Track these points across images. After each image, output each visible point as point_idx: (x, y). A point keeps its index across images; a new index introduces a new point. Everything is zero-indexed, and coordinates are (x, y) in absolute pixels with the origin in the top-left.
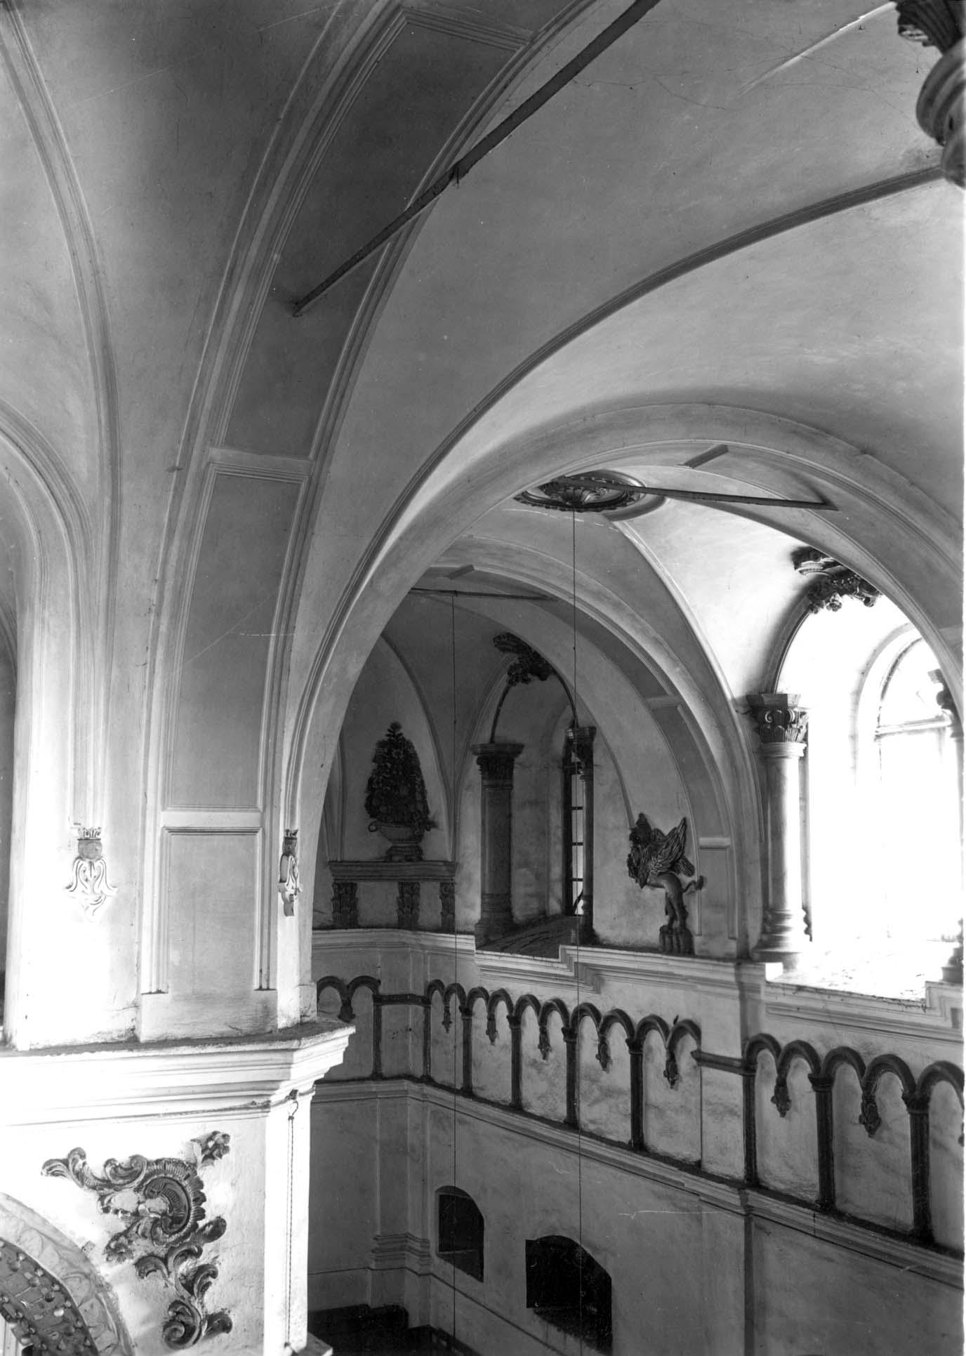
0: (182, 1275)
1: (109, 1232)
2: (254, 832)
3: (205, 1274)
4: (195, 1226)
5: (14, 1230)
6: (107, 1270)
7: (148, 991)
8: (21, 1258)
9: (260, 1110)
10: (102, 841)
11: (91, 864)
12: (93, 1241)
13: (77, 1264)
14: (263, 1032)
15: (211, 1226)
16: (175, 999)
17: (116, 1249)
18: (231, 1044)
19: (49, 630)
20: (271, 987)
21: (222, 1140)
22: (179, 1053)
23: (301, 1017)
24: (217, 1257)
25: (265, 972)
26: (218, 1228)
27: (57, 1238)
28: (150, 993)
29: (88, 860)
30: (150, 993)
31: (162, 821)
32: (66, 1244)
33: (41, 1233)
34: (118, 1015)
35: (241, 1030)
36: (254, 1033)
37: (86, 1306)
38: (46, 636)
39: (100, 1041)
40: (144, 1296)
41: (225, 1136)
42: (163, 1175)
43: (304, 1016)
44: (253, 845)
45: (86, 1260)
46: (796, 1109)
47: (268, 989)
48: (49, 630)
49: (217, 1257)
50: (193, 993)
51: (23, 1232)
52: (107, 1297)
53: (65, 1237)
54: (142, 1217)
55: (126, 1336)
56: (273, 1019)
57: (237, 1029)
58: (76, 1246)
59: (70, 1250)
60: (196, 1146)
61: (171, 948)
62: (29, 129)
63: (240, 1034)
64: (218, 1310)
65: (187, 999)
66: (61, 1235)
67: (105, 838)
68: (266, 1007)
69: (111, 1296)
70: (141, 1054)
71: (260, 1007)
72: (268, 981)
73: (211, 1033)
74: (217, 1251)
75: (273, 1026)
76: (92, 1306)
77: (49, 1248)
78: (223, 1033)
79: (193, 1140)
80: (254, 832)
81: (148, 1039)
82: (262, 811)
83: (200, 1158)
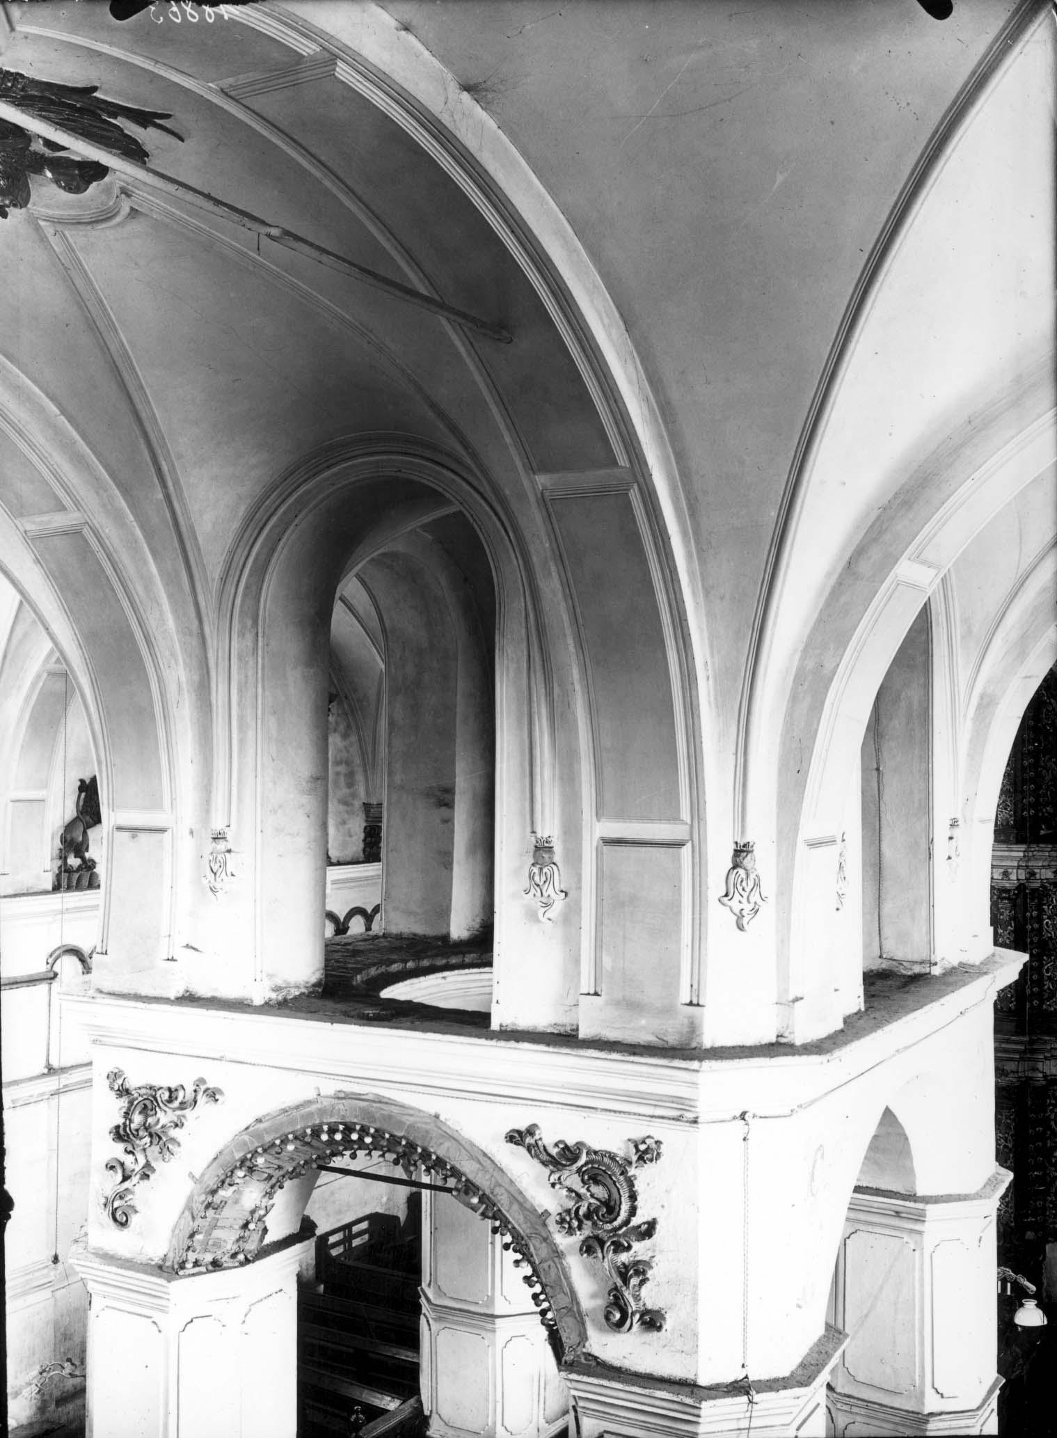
0: (623, 1264)
1: (562, 1206)
2: (680, 844)
3: (639, 1270)
4: (627, 1222)
5: (488, 1183)
6: (563, 1241)
7: (587, 992)
8: (495, 1209)
9: (688, 1124)
10: (555, 849)
11: (541, 869)
12: (550, 1211)
13: (537, 1227)
14: (688, 1047)
15: (646, 1226)
16: (607, 1004)
17: (568, 1221)
18: (634, 1054)
19: (507, 656)
20: (701, 1003)
21: (654, 1146)
22: (587, 1054)
23: (778, 1036)
24: (653, 1257)
25: (695, 986)
26: (648, 1230)
27: (521, 1200)
28: (589, 994)
29: (538, 866)
30: (589, 994)
31: (598, 831)
32: (528, 1206)
33: (508, 1192)
34: (570, 1010)
35: (667, 1042)
36: (679, 1047)
37: (545, 1265)
38: (505, 662)
39: (556, 1032)
40: (593, 1273)
41: (658, 1143)
42: (597, 1166)
43: (782, 1036)
44: (678, 859)
45: (545, 1225)
46: (420, 6)
47: (698, 1005)
48: (507, 656)
49: (653, 1257)
50: (624, 999)
51: (495, 1186)
52: (561, 1264)
53: (527, 1200)
54: (583, 1200)
55: (578, 1304)
56: (699, 1035)
57: (664, 1040)
58: (536, 1210)
59: (531, 1212)
60: (631, 1146)
61: (604, 953)
62: (646, 382)
63: (666, 1046)
64: (656, 1308)
65: (617, 1003)
66: (524, 1197)
67: (558, 848)
68: (692, 1023)
69: (565, 1264)
70: (556, 1050)
71: (686, 1021)
72: (698, 996)
73: (639, 1041)
74: (654, 1251)
75: (698, 1043)
76: (549, 1267)
77: (515, 1207)
78: (650, 1042)
79: (629, 1140)
80: (680, 844)
81: (585, 1037)
82: (689, 821)
83: (634, 1158)
